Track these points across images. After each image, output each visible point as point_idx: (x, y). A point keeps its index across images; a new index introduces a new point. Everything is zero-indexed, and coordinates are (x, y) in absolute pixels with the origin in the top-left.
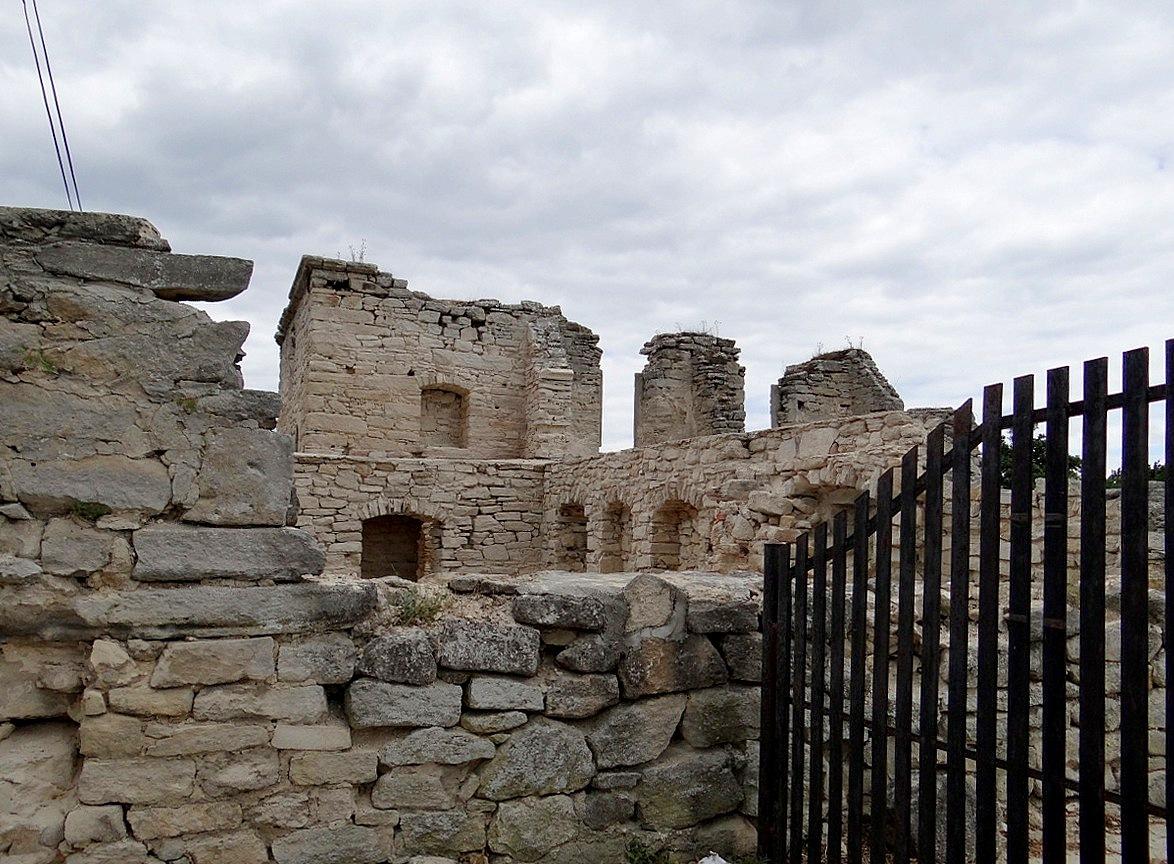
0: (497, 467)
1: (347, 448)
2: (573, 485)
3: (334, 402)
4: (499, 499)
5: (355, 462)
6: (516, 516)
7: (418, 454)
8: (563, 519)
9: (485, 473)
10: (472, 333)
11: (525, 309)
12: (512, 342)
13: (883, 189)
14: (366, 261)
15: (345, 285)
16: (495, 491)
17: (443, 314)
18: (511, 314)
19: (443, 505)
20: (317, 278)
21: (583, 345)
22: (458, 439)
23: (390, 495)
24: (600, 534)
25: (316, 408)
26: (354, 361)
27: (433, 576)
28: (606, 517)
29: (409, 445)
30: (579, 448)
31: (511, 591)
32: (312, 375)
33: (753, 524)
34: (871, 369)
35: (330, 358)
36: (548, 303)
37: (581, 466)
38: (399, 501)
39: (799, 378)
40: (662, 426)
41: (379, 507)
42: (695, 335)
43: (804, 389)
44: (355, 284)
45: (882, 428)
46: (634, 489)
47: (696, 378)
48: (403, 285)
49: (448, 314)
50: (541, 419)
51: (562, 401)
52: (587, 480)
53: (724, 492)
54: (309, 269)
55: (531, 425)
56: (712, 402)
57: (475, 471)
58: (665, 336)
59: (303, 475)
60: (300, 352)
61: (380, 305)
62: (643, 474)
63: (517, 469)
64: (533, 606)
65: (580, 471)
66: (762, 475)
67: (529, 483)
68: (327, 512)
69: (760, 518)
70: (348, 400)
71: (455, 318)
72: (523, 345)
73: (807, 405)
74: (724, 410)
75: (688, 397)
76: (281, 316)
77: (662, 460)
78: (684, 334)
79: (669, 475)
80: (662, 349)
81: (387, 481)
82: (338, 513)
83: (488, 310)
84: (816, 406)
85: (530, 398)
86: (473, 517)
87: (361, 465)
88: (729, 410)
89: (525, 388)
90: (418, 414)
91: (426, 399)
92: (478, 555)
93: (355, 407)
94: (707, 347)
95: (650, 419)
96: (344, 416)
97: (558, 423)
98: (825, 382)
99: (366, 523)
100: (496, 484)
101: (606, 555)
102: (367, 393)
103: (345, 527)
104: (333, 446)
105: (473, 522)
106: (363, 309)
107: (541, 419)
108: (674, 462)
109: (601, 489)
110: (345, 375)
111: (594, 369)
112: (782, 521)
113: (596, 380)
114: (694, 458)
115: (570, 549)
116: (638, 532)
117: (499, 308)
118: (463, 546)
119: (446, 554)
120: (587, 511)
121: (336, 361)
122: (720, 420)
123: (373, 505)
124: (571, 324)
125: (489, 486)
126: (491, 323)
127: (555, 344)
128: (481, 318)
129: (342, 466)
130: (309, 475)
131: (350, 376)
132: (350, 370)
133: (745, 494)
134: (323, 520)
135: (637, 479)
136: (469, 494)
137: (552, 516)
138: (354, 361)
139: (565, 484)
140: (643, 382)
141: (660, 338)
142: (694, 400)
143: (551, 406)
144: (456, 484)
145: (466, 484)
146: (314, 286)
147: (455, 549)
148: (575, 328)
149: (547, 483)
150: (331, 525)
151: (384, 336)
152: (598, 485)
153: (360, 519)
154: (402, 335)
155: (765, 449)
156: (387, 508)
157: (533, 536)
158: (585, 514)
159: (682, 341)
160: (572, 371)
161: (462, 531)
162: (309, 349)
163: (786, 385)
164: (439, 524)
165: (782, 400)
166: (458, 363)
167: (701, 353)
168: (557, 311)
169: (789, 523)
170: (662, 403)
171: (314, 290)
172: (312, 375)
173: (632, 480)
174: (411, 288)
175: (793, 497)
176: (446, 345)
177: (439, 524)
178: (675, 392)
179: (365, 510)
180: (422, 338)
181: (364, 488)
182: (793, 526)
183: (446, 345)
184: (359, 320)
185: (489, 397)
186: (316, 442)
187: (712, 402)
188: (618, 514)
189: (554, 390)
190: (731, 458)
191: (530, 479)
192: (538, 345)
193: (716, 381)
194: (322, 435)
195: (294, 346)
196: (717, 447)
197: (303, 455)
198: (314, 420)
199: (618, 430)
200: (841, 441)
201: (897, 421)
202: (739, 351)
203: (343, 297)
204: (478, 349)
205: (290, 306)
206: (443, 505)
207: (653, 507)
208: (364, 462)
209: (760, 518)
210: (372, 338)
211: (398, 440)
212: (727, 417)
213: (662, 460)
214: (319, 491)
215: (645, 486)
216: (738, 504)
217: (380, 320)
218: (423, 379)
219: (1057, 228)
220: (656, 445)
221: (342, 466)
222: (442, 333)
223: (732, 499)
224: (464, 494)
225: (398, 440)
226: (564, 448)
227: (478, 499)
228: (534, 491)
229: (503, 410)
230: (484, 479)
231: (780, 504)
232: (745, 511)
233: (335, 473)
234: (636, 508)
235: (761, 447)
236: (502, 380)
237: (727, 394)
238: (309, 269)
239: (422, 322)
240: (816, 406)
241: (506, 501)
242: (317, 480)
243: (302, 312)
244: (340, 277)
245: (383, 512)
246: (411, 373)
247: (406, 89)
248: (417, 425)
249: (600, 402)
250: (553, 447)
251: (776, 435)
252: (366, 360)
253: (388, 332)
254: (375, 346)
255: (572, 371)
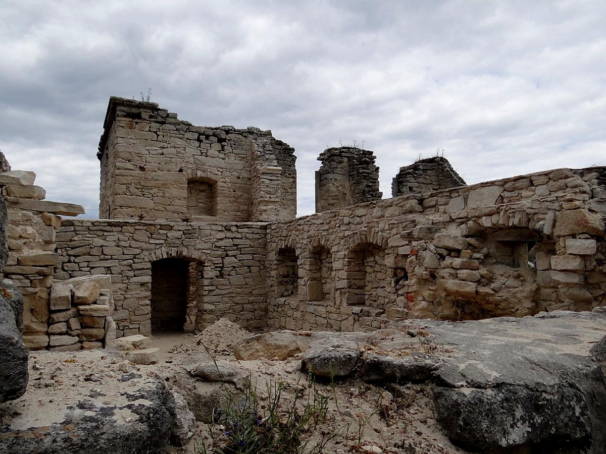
0: (237, 226)
1: (141, 217)
2: (287, 236)
3: (132, 189)
4: (239, 246)
5: (145, 225)
6: (250, 257)
7: (186, 220)
8: (279, 258)
9: (230, 230)
10: (217, 146)
11: (250, 132)
12: (242, 152)
13: (410, 98)
14: (151, 101)
15: (138, 116)
16: (236, 242)
17: (200, 134)
18: (241, 134)
19: (203, 251)
20: (120, 110)
21: (286, 154)
22: (211, 211)
23: (169, 245)
24: (307, 267)
25: (120, 192)
26: (144, 163)
27: (258, 339)
28: (311, 256)
29: (181, 215)
30: (284, 216)
31: (424, 375)
32: (117, 172)
33: (439, 257)
34: (449, 168)
35: (129, 161)
36: (264, 129)
37: (292, 224)
38: (175, 249)
39: (409, 173)
40: (332, 202)
41: (162, 253)
42: (351, 148)
43: (412, 180)
44: (145, 115)
45: (548, 182)
46: (333, 237)
47: (351, 174)
48: (175, 116)
49: (203, 134)
50: (262, 197)
51: (275, 186)
52: (297, 233)
53: (416, 234)
54: (115, 104)
55: (255, 201)
56: (362, 187)
57: (224, 229)
58: (332, 149)
59: (111, 234)
60: (111, 159)
61: (161, 128)
62: (339, 227)
63: (249, 227)
64: (490, 414)
65: (292, 228)
66: (439, 222)
67: (257, 236)
68: (128, 257)
69: (445, 252)
70: (141, 187)
71: (207, 137)
72: (249, 153)
73: (414, 189)
74: (370, 191)
75: (347, 184)
76: (99, 141)
77: (354, 216)
78: (343, 148)
79: (360, 226)
80: (330, 157)
81: (167, 236)
82: (135, 258)
83: (228, 132)
84: (419, 190)
85: (255, 185)
86: (223, 258)
87: (151, 227)
88: (373, 191)
89: (250, 181)
90: (186, 195)
91: (190, 187)
92: (226, 282)
93: (146, 191)
94: (357, 155)
95: (325, 197)
96: (139, 197)
97: (273, 200)
98: (423, 176)
99: (154, 264)
100: (237, 237)
101: (312, 281)
102: (153, 183)
103: (140, 266)
104: (132, 216)
105: (223, 261)
106: (150, 131)
107: (262, 197)
108: (364, 218)
109: (308, 238)
110: (138, 172)
111: (292, 167)
112: (462, 254)
113: (293, 175)
114: (380, 214)
115: (284, 277)
116: (336, 265)
117: (234, 131)
118: (217, 276)
119: (206, 282)
120: (298, 252)
121: (133, 163)
122: (368, 197)
123: (158, 252)
124: (277, 141)
125: (232, 239)
126: (229, 140)
127: (269, 152)
128: (223, 137)
129: (137, 227)
130: (115, 233)
131: (142, 172)
132: (142, 169)
133: (430, 236)
134: (125, 262)
135: (335, 230)
136: (220, 244)
137: (273, 256)
138: (144, 163)
139: (281, 236)
140: (319, 175)
141: (329, 150)
142: (351, 186)
143: (269, 189)
144: (212, 237)
145: (219, 238)
146: (118, 116)
147: (212, 279)
148: (280, 143)
149: (269, 236)
150: (130, 266)
151: (163, 148)
152: (305, 235)
153: (150, 261)
154: (175, 147)
155: (437, 204)
156: (167, 253)
157: (260, 269)
158: (297, 255)
159: (343, 152)
160: (280, 168)
161: (216, 267)
162: (116, 156)
163: (401, 178)
164: (201, 263)
165: (399, 186)
166: (209, 165)
167: (354, 158)
168: (269, 133)
169: (468, 256)
170: (333, 189)
171: (118, 118)
172: (117, 172)
173: (331, 231)
174: (180, 118)
175: (467, 236)
176: (202, 153)
177: (201, 263)
178: (339, 182)
179: (153, 255)
180: (187, 149)
181: (152, 241)
182: (471, 258)
183: (202, 153)
184: (148, 138)
185: (229, 185)
186: (121, 213)
187: (362, 187)
188: (320, 253)
189: (270, 180)
190: (411, 212)
191: (258, 234)
192: (259, 153)
193: (365, 174)
194: (125, 209)
195: (107, 158)
196: (399, 205)
197: (111, 220)
198: (120, 200)
199: (306, 202)
200: (506, 194)
201: (563, 176)
202: (375, 157)
203: (137, 123)
204: (222, 156)
205: (105, 133)
206: (203, 251)
207: (348, 248)
208: (151, 225)
209: (445, 252)
210: (156, 149)
211: (173, 212)
212: (372, 195)
213: (354, 216)
214: (122, 243)
215: (341, 235)
216: (425, 243)
217: (160, 138)
218: (188, 173)
219: (492, 116)
220: (349, 207)
221: (137, 227)
222: (200, 146)
223: (421, 239)
224: (216, 244)
225: (173, 212)
226: (277, 215)
227: (225, 246)
228: (260, 241)
229: (238, 193)
230: (229, 234)
231: (460, 242)
232: (432, 248)
233: (133, 232)
234: (334, 249)
235: (433, 203)
236: (237, 174)
237: (371, 182)
238: (115, 104)
239: (187, 139)
240: (419, 190)
241: (243, 248)
242: (121, 237)
243: (112, 136)
244: (134, 110)
245: (165, 256)
246: (181, 171)
247: (175, 49)
248: (185, 202)
249: (296, 188)
250: (270, 214)
251: (446, 194)
252: (152, 162)
253: (166, 145)
254: (157, 154)
255: (280, 168)
